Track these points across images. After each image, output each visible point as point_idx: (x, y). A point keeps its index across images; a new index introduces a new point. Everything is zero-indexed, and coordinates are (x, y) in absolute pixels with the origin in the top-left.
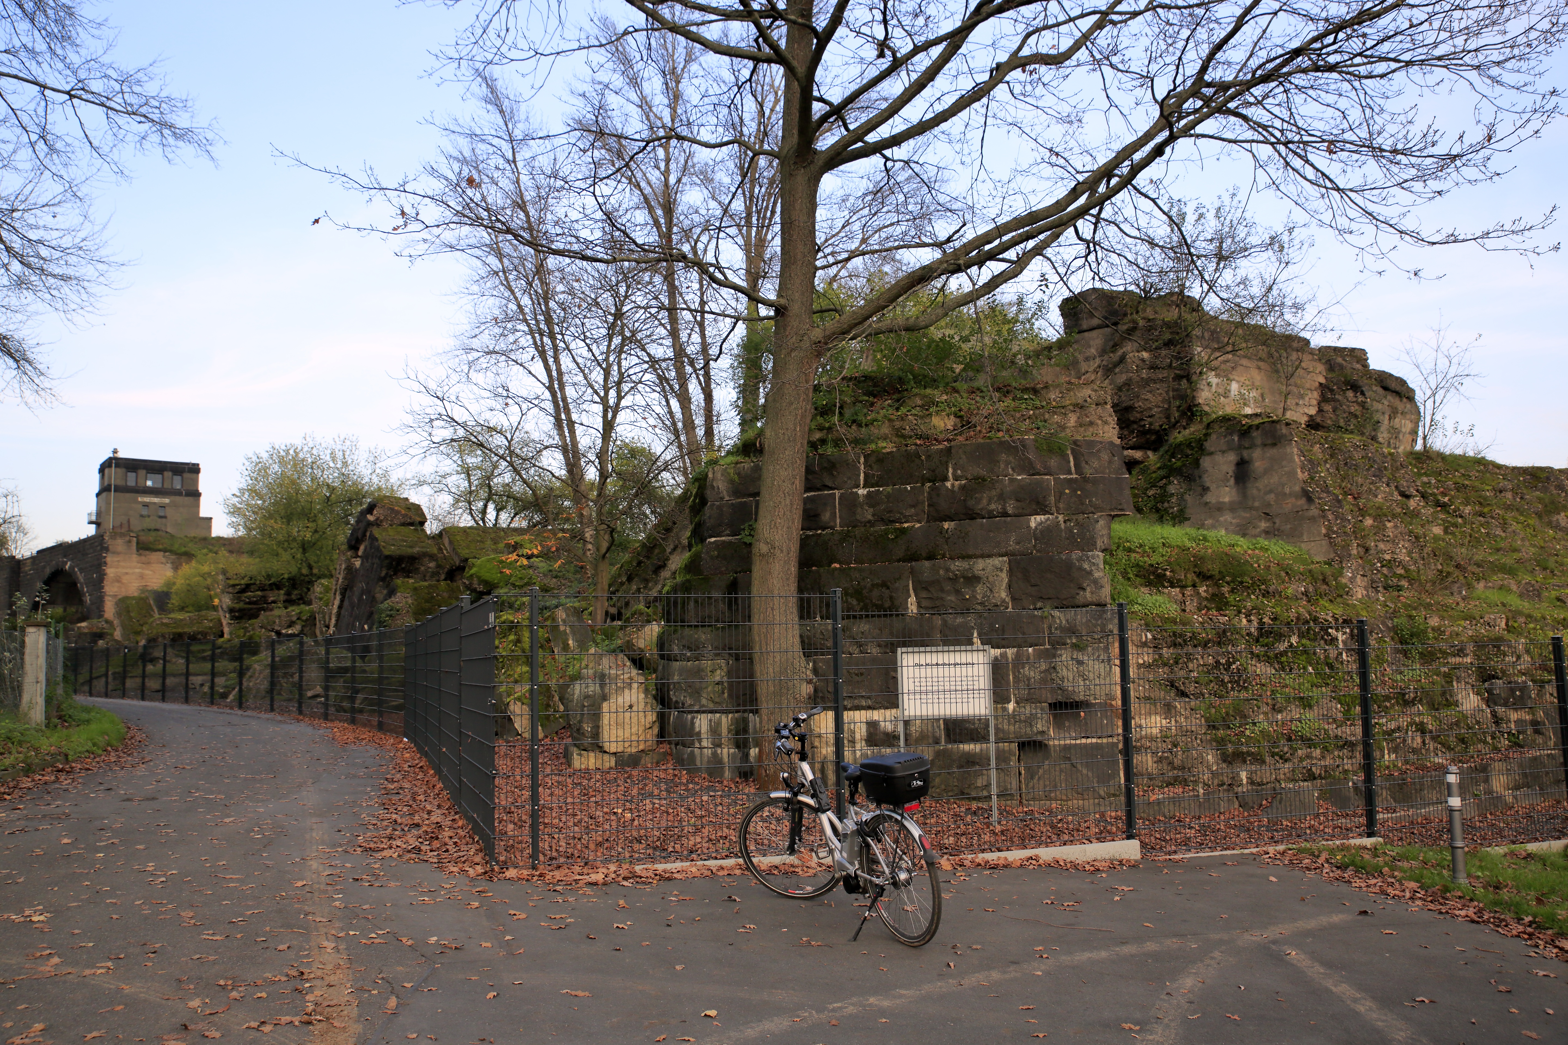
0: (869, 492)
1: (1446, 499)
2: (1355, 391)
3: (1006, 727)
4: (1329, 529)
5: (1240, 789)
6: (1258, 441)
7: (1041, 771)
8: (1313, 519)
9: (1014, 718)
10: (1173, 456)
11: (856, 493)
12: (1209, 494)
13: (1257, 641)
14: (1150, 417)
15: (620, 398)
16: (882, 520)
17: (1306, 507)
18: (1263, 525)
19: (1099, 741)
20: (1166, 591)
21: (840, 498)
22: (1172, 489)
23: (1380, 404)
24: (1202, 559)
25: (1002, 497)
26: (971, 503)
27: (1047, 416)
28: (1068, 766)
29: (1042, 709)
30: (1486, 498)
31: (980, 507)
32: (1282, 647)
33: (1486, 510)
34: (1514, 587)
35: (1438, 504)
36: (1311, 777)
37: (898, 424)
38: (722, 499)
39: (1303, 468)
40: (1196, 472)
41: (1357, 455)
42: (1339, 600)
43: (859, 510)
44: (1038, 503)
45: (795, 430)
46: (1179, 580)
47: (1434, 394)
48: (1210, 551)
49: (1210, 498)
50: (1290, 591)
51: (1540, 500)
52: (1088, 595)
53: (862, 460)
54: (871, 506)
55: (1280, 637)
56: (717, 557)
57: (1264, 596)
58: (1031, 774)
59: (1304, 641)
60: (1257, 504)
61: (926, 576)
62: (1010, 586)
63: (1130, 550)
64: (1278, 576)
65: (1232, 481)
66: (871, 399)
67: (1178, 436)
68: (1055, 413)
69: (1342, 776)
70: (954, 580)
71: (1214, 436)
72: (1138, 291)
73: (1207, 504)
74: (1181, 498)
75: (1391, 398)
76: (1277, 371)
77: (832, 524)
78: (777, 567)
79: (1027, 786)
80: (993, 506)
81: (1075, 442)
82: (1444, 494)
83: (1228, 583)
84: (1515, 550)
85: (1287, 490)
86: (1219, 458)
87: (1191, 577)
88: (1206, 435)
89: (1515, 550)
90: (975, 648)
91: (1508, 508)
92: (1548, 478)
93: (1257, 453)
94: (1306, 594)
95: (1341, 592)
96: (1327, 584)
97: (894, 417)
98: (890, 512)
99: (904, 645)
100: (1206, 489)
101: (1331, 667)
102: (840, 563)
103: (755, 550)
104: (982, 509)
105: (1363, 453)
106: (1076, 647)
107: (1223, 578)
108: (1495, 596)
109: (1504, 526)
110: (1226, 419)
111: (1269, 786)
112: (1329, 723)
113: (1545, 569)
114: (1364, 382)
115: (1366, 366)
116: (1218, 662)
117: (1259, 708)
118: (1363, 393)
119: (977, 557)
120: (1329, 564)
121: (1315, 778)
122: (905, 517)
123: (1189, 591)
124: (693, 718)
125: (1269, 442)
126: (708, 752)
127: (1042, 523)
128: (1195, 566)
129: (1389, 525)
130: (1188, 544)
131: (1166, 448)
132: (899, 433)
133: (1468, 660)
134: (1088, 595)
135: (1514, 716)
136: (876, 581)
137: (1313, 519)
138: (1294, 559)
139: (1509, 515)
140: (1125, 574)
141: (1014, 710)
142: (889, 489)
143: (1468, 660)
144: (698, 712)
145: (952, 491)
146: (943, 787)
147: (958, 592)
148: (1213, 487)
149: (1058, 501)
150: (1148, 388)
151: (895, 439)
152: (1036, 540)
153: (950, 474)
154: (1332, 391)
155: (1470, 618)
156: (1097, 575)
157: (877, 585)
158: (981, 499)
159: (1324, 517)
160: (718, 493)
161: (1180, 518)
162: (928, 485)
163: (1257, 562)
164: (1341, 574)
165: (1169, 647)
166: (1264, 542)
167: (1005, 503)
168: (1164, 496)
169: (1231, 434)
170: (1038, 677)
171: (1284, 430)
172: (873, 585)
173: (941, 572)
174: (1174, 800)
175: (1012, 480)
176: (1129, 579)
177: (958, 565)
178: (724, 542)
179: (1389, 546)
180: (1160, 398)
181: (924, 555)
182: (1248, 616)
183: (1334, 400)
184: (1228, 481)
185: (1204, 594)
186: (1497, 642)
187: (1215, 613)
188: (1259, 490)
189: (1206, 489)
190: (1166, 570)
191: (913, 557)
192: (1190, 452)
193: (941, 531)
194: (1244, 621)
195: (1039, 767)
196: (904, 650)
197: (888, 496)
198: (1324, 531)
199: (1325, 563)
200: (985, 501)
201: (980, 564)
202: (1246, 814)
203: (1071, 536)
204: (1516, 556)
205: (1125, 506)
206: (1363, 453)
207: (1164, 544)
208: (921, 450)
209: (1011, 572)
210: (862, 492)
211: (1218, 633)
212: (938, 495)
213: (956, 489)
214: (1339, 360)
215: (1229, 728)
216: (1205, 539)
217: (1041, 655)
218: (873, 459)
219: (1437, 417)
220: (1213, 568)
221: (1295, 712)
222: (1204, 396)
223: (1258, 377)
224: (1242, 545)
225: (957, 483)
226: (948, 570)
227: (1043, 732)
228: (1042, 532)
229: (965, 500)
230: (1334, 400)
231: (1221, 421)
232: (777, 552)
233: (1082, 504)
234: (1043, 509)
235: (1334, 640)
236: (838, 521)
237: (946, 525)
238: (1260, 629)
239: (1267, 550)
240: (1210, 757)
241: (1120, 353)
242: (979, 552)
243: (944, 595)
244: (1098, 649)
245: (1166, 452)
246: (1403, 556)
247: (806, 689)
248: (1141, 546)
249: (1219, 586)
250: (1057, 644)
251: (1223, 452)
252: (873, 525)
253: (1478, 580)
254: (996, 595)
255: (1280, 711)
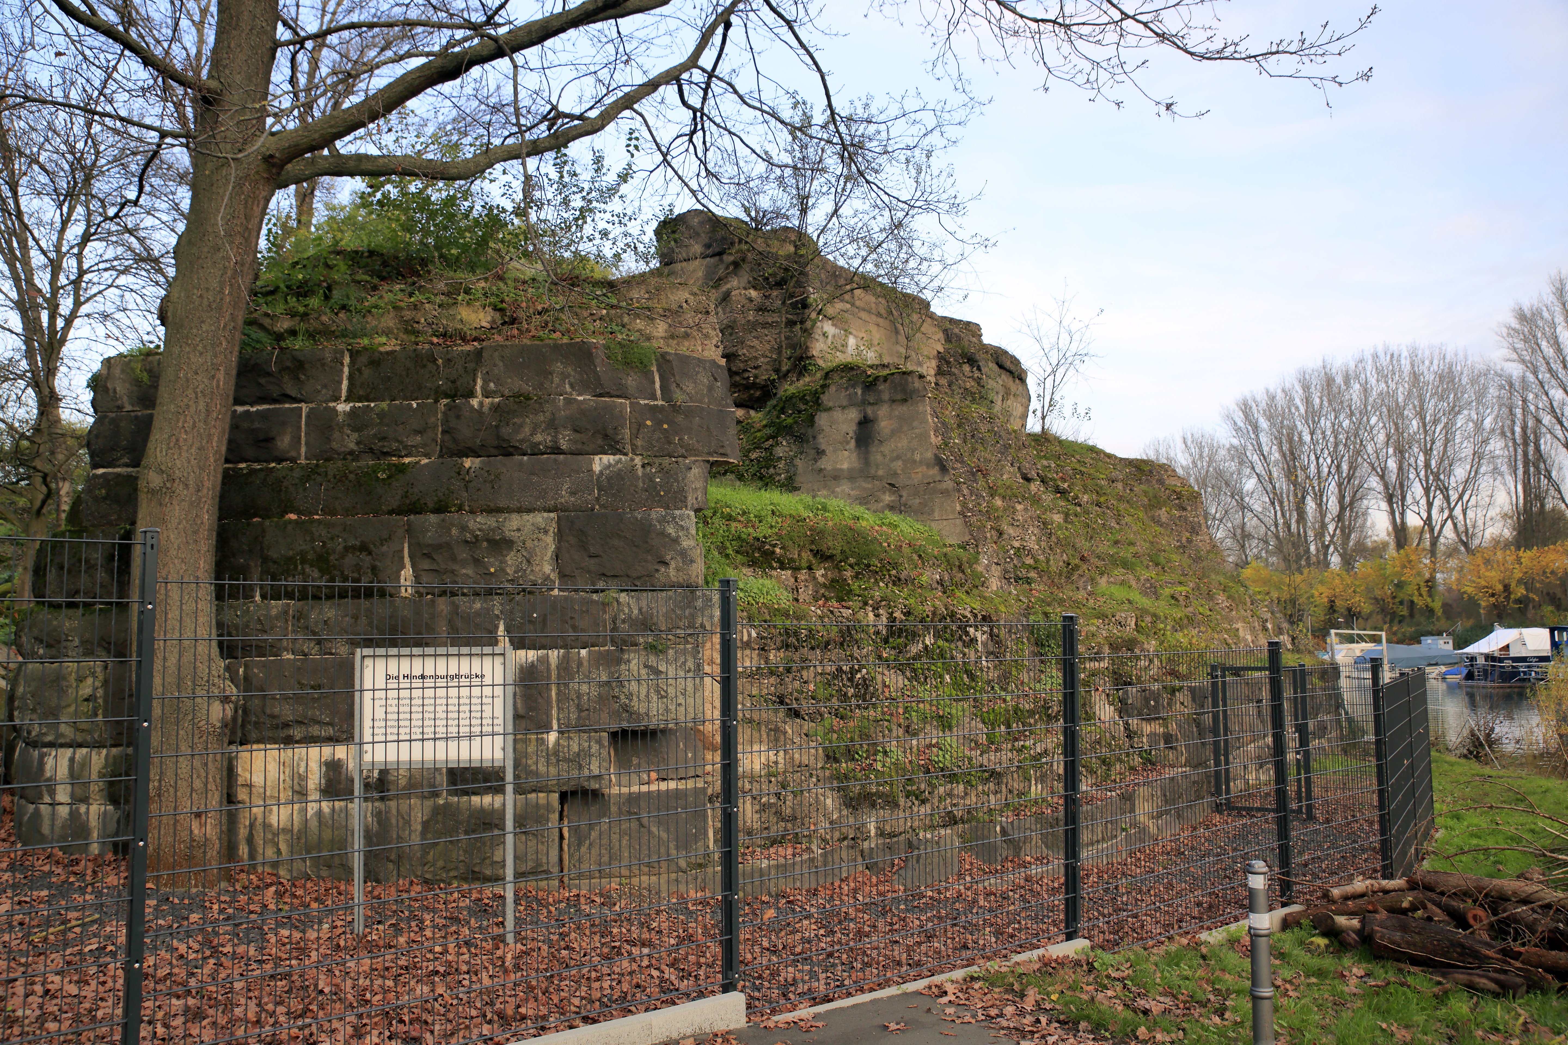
0: (353, 409)
1: (1066, 485)
2: (972, 366)
3: (542, 768)
4: (964, 505)
5: (866, 845)
6: (886, 396)
7: (594, 834)
8: (946, 493)
9: (556, 755)
10: (783, 411)
11: (334, 409)
12: (824, 458)
13: (886, 641)
14: (755, 368)
15: (78, 304)
16: (371, 450)
17: (938, 478)
18: (888, 498)
19: (681, 785)
20: (774, 573)
21: (308, 416)
22: (779, 452)
23: (996, 382)
24: (821, 532)
25: (552, 425)
26: (505, 431)
27: (626, 319)
28: (634, 825)
29: (599, 742)
30: (1101, 487)
31: (520, 437)
32: (915, 649)
33: (1102, 499)
34: (1133, 583)
35: (1058, 491)
36: (951, 820)
37: (408, 314)
38: (120, 408)
39: (936, 431)
40: (810, 432)
41: (984, 427)
42: (975, 591)
43: (336, 435)
44: (606, 436)
45: (221, 291)
46: (792, 560)
47: (1054, 372)
48: (830, 523)
49: (825, 463)
50: (924, 578)
51: (1146, 493)
52: (672, 573)
53: (347, 360)
54: (355, 429)
55: (914, 636)
56: (104, 499)
57: (894, 584)
58: (579, 837)
59: (940, 643)
60: (881, 473)
61: (430, 536)
62: (557, 556)
63: (730, 518)
64: (910, 559)
65: (853, 443)
66: (376, 281)
67: (789, 388)
68: (637, 316)
69: (986, 817)
70: (473, 543)
71: (833, 389)
72: (747, 219)
73: (821, 470)
74: (791, 462)
75: (1005, 378)
76: (897, 332)
77: (293, 454)
78: (176, 512)
79: (571, 856)
80: (539, 438)
81: (663, 356)
82: (1063, 480)
83: (851, 566)
84: (1132, 544)
85: (917, 457)
86: (837, 415)
87: (806, 556)
88: (824, 386)
89: (1132, 544)
90: (497, 650)
91: (1120, 499)
92: (1151, 472)
93: (883, 411)
94: (941, 582)
95: (977, 583)
96: (963, 572)
97: (402, 304)
98: (384, 439)
99: (369, 643)
100: (820, 453)
101: (972, 676)
102: (299, 513)
103: (142, 484)
104: (522, 441)
105: (988, 426)
106: (652, 648)
107: (846, 559)
108: (1120, 593)
109: (1118, 517)
110: (847, 368)
111: (902, 838)
112: (971, 749)
113: (1157, 565)
114: (980, 356)
115: (981, 341)
116: (839, 670)
117: (890, 731)
118: (979, 369)
119: (510, 511)
120: (964, 548)
121: (956, 823)
122: (406, 447)
123: (803, 575)
124: (42, 756)
125: (899, 397)
126: (63, 811)
127: (610, 465)
128: (812, 542)
129: (1019, 507)
130: (805, 514)
131: (773, 402)
132: (409, 328)
133: (1104, 664)
134: (672, 572)
135: (1147, 728)
136: (352, 542)
137: (946, 493)
138: (925, 539)
139: (1122, 507)
140: (722, 549)
141: (557, 743)
142: (384, 405)
143: (1104, 664)
144: (51, 745)
145: (480, 412)
146: (440, 863)
147: (477, 562)
148: (829, 450)
149: (635, 436)
150: (754, 334)
151: (402, 336)
152: (599, 490)
153: (478, 388)
154: (948, 363)
155: (1103, 616)
156: (686, 543)
157: (353, 548)
158: (521, 426)
159: (959, 491)
160: (115, 399)
161: (790, 486)
162: (445, 401)
163: (886, 540)
164: (977, 561)
165: (779, 649)
166: (894, 518)
167: (557, 433)
168: (770, 461)
169: (854, 386)
170: (594, 693)
171: (917, 384)
172: (347, 549)
173: (454, 531)
174: (782, 868)
175: (569, 401)
176: (727, 556)
177: (480, 522)
178: (118, 475)
179: (1019, 531)
180: (768, 347)
181: (431, 505)
182: (875, 608)
183: (950, 373)
184: (848, 443)
185: (821, 580)
186: (1131, 644)
187: (835, 604)
188: (884, 456)
189: (820, 453)
190: (775, 546)
191: (415, 508)
192: (803, 407)
193: (460, 471)
194: (871, 615)
195: (591, 827)
196: (367, 651)
197: (382, 415)
198: (958, 508)
199: (960, 547)
200: (527, 430)
201: (514, 522)
202: (874, 879)
203: (651, 488)
204: (1132, 549)
205: (728, 450)
206: (988, 426)
207: (773, 513)
208: (436, 351)
209: (560, 535)
210: (343, 407)
211: (841, 631)
212: (458, 417)
213: (485, 409)
214: (956, 331)
215: (853, 759)
216: (825, 509)
217: (599, 660)
218: (363, 359)
219: (1057, 397)
220: (834, 545)
221: (933, 734)
222: (818, 347)
223: (877, 335)
224: (868, 520)
225: (488, 401)
226: (464, 528)
227: (599, 777)
228: (609, 479)
229: (497, 427)
230: (950, 373)
231: (842, 370)
232: (179, 488)
233: (670, 443)
234: (612, 446)
235: (974, 640)
236: (303, 449)
237: (468, 463)
238: (890, 628)
239: (896, 526)
240: (829, 802)
241: (724, 288)
242: (514, 504)
243: (456, 567)
244: (684, 652)
245: (774, 407)
246: (1032, 545)
247: (217, 712)
248: (744, 513)
249: (840, 570)
250: (624, 644)
251: (843, 408)
252: (356, 459)
253: (1102, 574)
254: (537, 569)
255: (915, 735)
